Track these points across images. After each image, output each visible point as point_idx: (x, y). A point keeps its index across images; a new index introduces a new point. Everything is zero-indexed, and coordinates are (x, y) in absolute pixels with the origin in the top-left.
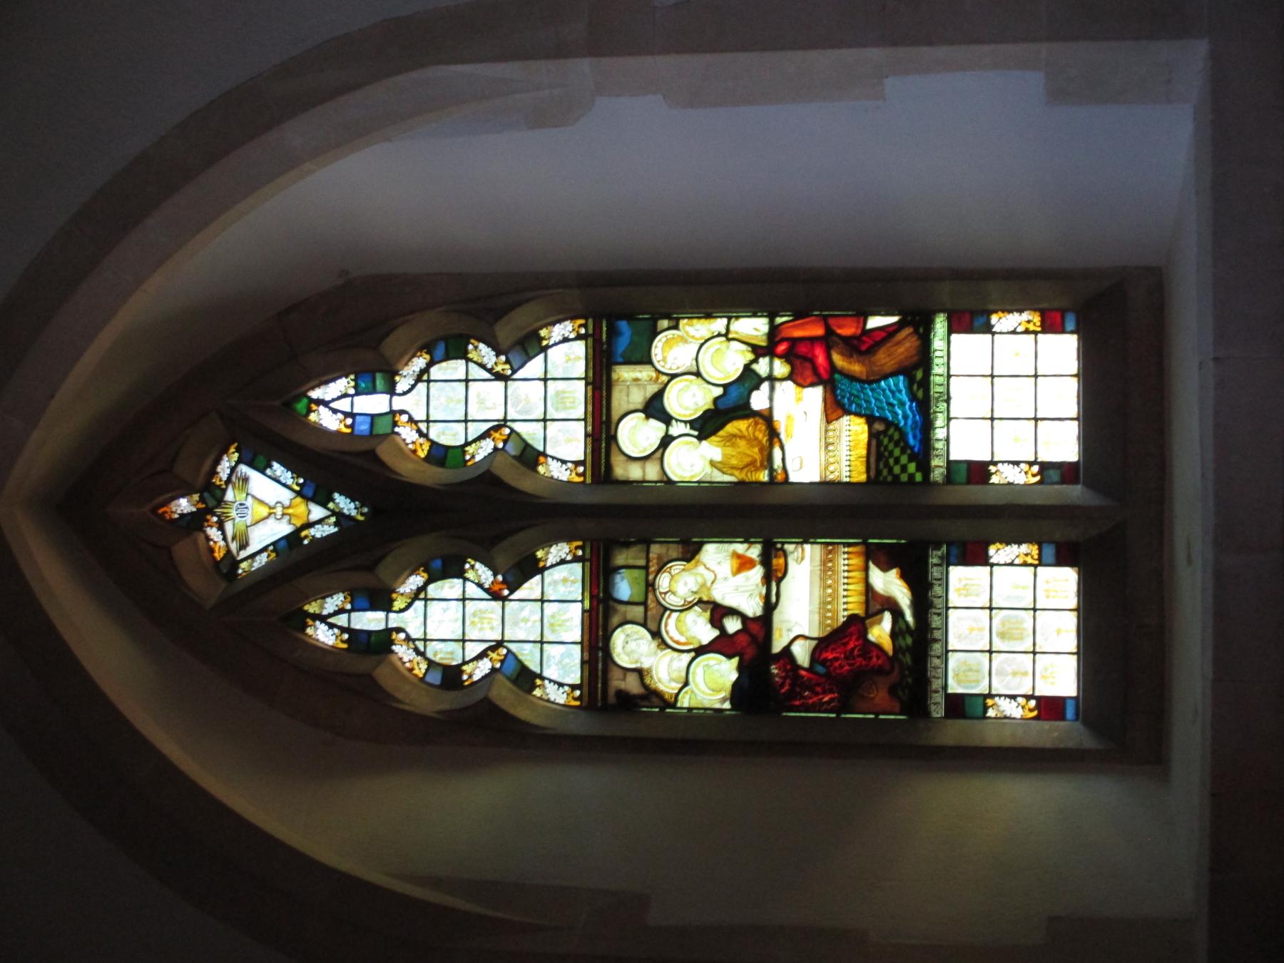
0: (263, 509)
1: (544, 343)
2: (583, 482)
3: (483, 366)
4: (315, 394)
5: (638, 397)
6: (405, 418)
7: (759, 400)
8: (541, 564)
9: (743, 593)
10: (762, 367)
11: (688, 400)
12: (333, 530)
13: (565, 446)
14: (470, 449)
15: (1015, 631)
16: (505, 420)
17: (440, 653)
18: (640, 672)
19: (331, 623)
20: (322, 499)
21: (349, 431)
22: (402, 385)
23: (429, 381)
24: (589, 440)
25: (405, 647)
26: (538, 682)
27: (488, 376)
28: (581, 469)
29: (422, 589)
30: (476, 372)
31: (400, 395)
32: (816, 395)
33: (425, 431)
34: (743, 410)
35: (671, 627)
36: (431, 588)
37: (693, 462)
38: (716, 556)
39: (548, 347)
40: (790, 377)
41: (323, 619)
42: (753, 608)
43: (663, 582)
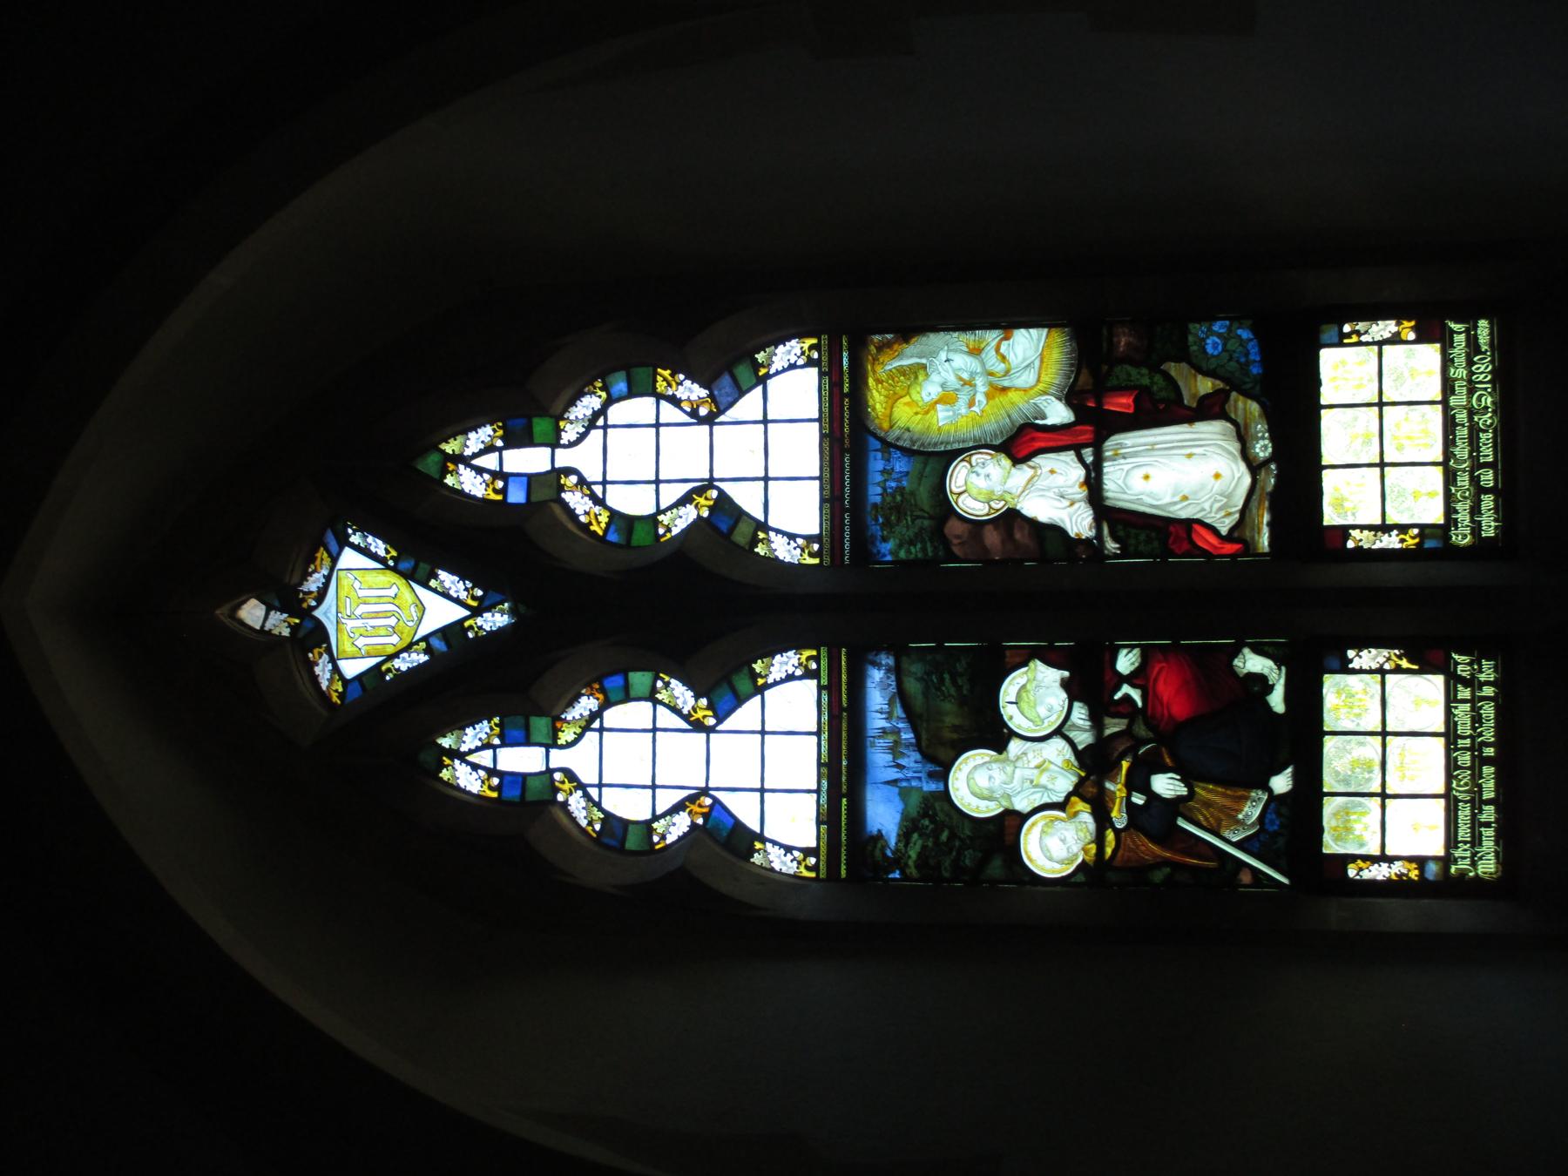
1: (763, 372)
2: (817, 879)
3: (675, 710)
4: (450, 447)
8: (761, 681)
14: (659, 826)
15: (1395, 768)
16: (712, 479)
19: (478, 760)
21: (499, 497)
22: (570, 433)
23: (601, 730)
24: (824, 770)
25: (578, 494)
26: (758, 845)
28: (812, 861)
29: (596, 715)
30: (666, 718)
31: (564, 446)
33: (596, 799)
36: (607, 714)
39: (768, 376)
41: (462, 757)
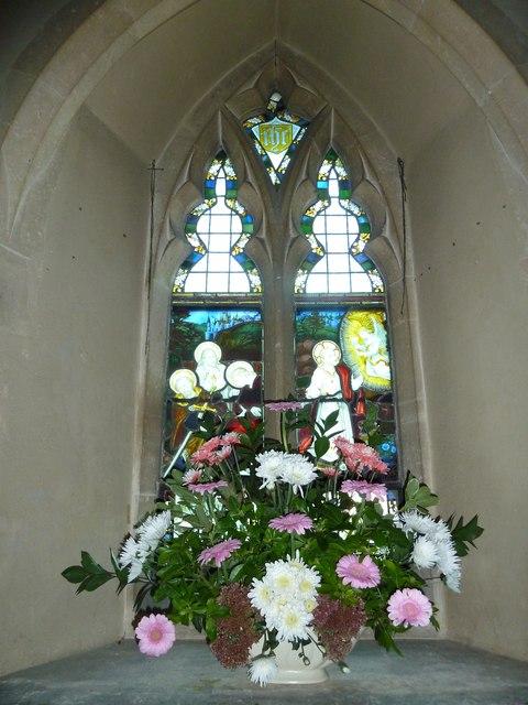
6: (327, 204)
12: (274, 182)
27: (234, 242)
28: (179, 290)
29: (237, 213)
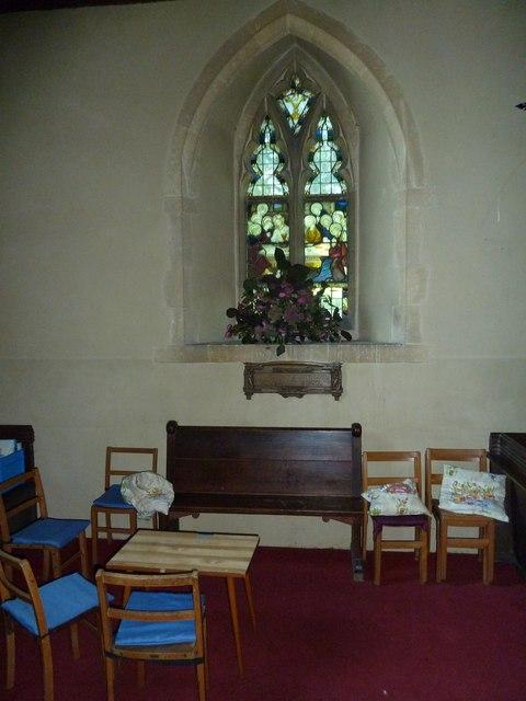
0: (296, 105)
5: (326, 207)
7: (325, 239)
9: (277, 237)
10: (334, 240)
11: (326, 221)
13: (313, 189)
17: (317, 155)
18: (256, 211)
20: (299, 123)
30: (276, 166)
32: (327, 254)
34: (323, 236)
35: (268, 219)
37: (309, 222)
38: (285, 230)
40: (331, 247)
42: (273, 239)
43: (279, 216)
